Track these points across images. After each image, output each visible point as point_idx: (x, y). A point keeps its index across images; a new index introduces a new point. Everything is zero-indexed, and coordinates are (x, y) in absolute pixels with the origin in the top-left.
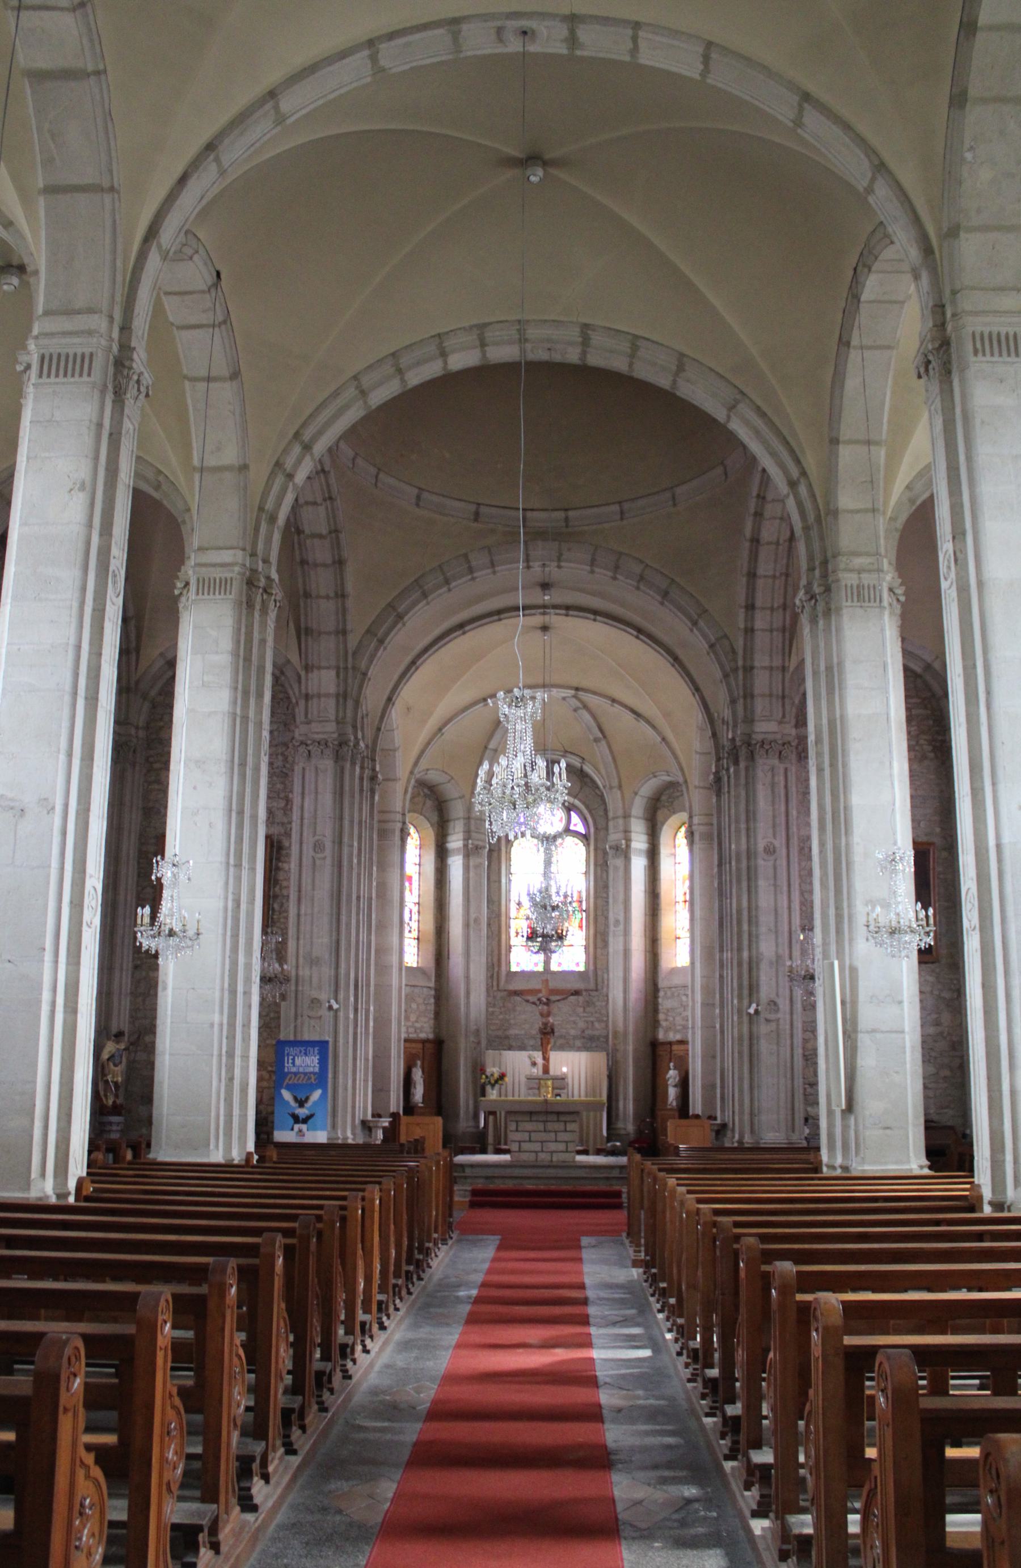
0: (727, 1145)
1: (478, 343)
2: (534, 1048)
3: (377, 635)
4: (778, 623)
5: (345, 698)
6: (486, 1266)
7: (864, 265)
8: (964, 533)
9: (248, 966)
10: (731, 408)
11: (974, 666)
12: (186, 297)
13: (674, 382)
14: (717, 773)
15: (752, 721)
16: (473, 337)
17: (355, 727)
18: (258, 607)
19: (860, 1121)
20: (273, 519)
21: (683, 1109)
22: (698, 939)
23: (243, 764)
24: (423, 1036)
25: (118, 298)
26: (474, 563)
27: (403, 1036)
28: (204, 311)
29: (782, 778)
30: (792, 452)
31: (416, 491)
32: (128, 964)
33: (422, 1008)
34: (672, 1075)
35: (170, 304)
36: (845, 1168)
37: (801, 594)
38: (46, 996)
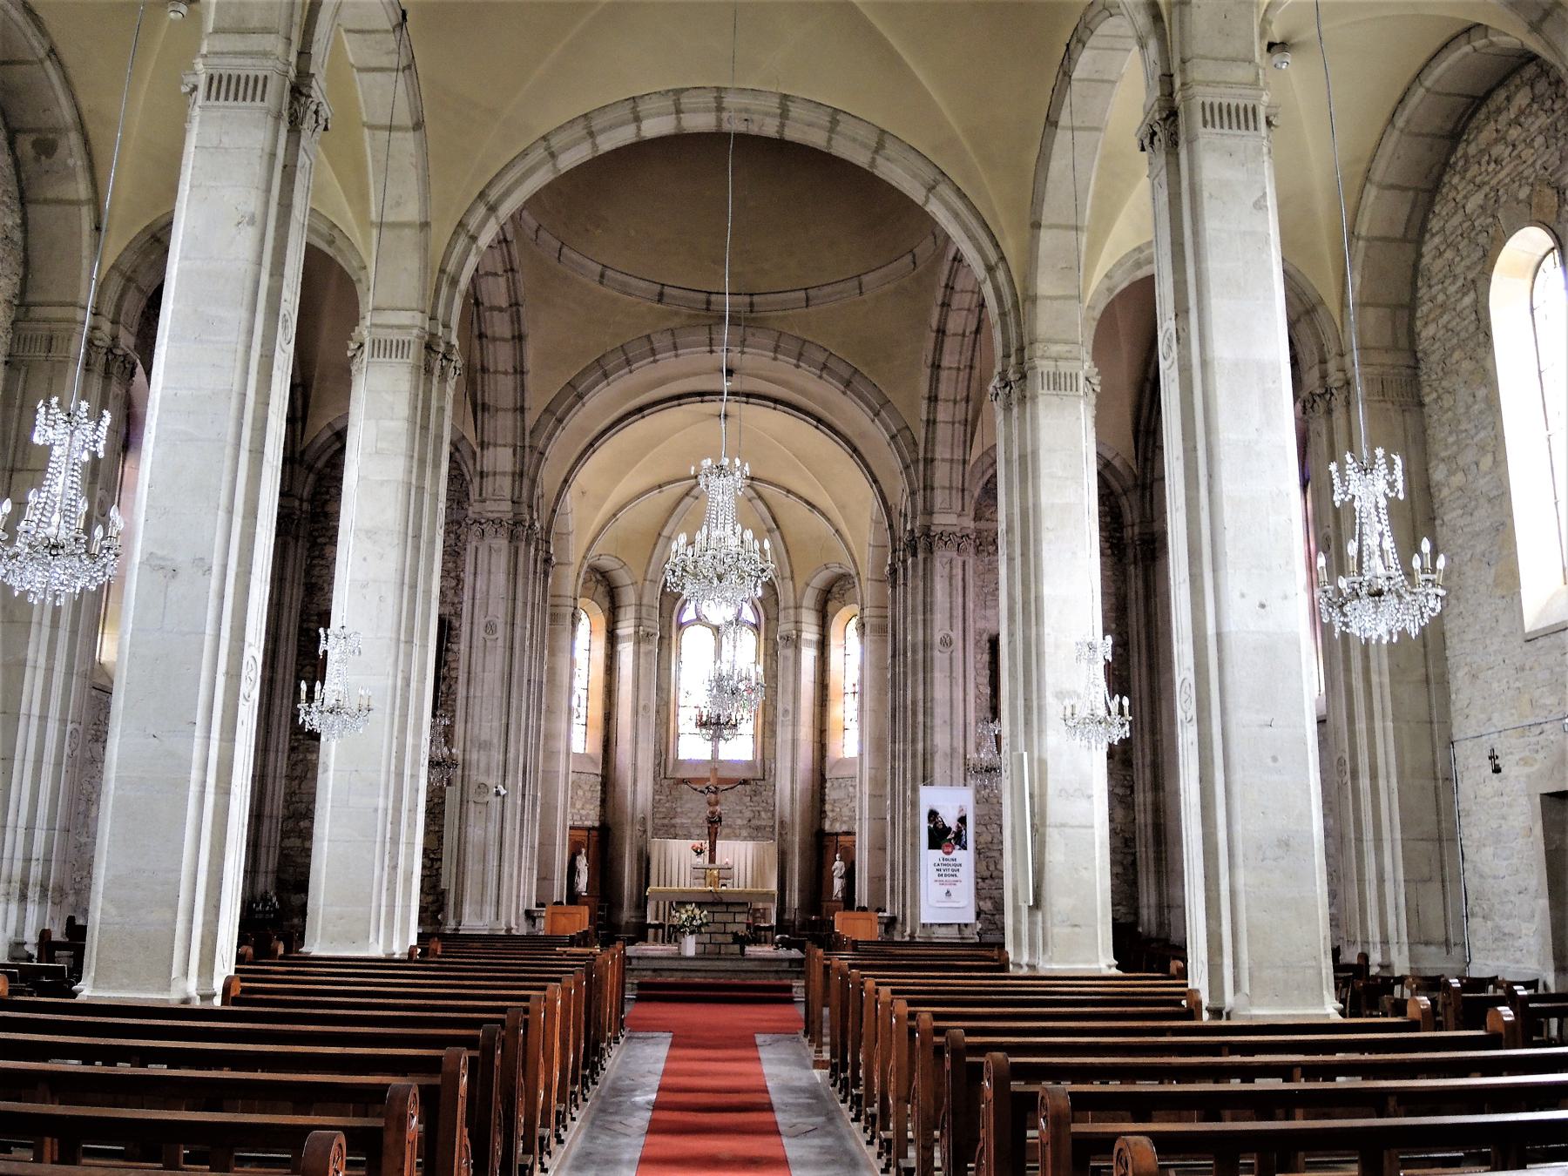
0: (897, 938)
1: (673, 109)
2: (699, 837)
3: (556, 414)
4: (960, 416)
5: (521, 475)
6: (661, 1066)
7: (1079, 41)
8: (1187, 311)
9: (417, 747)
10: (931, 189)
11: (1195, 448)
12: (367, 36)
13: (874, 159)
14: (892, 565)
15: (931, 513)
16: (668, 103)
17: (530, 507)
18: (437, 372)
19: (1048, 917)
20: (454, 282)
21: (849, 900)
22: (867, 730)
23: (417, 537)
24: (588, 823)
25: (297, 19)
26: (656, 345)
27: (569, 823)
28: (388, 53)
29: (960, 571)
30: (992, 236)
31: (600, 268)
32: (284, 745)
33: (589, 795)
34: (838, 866)
35: (349, 44)
36: (1032, 967)
37: (996, 381)
38: (195, 775)
